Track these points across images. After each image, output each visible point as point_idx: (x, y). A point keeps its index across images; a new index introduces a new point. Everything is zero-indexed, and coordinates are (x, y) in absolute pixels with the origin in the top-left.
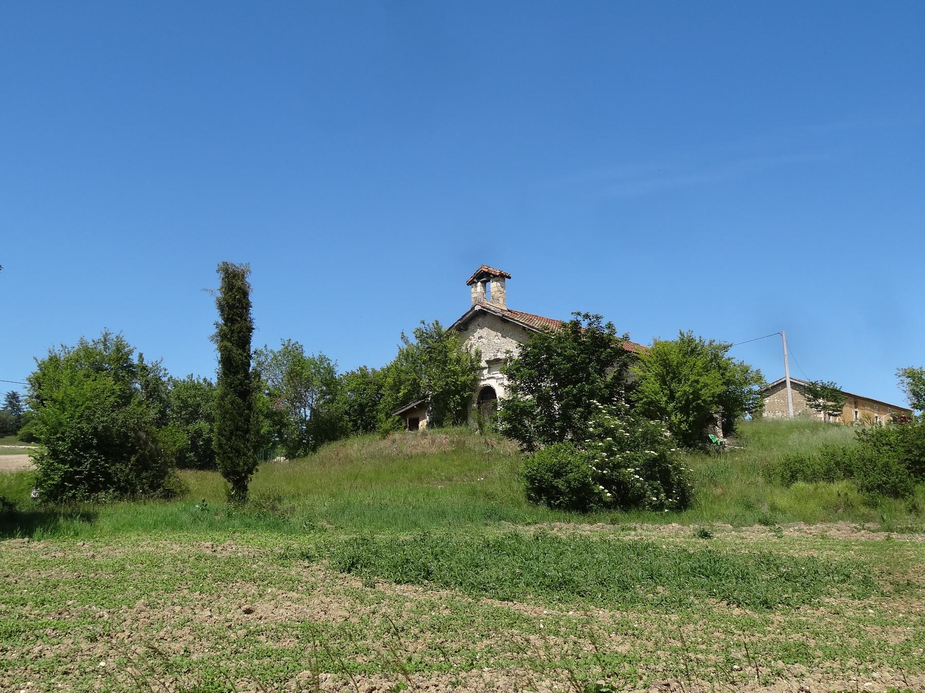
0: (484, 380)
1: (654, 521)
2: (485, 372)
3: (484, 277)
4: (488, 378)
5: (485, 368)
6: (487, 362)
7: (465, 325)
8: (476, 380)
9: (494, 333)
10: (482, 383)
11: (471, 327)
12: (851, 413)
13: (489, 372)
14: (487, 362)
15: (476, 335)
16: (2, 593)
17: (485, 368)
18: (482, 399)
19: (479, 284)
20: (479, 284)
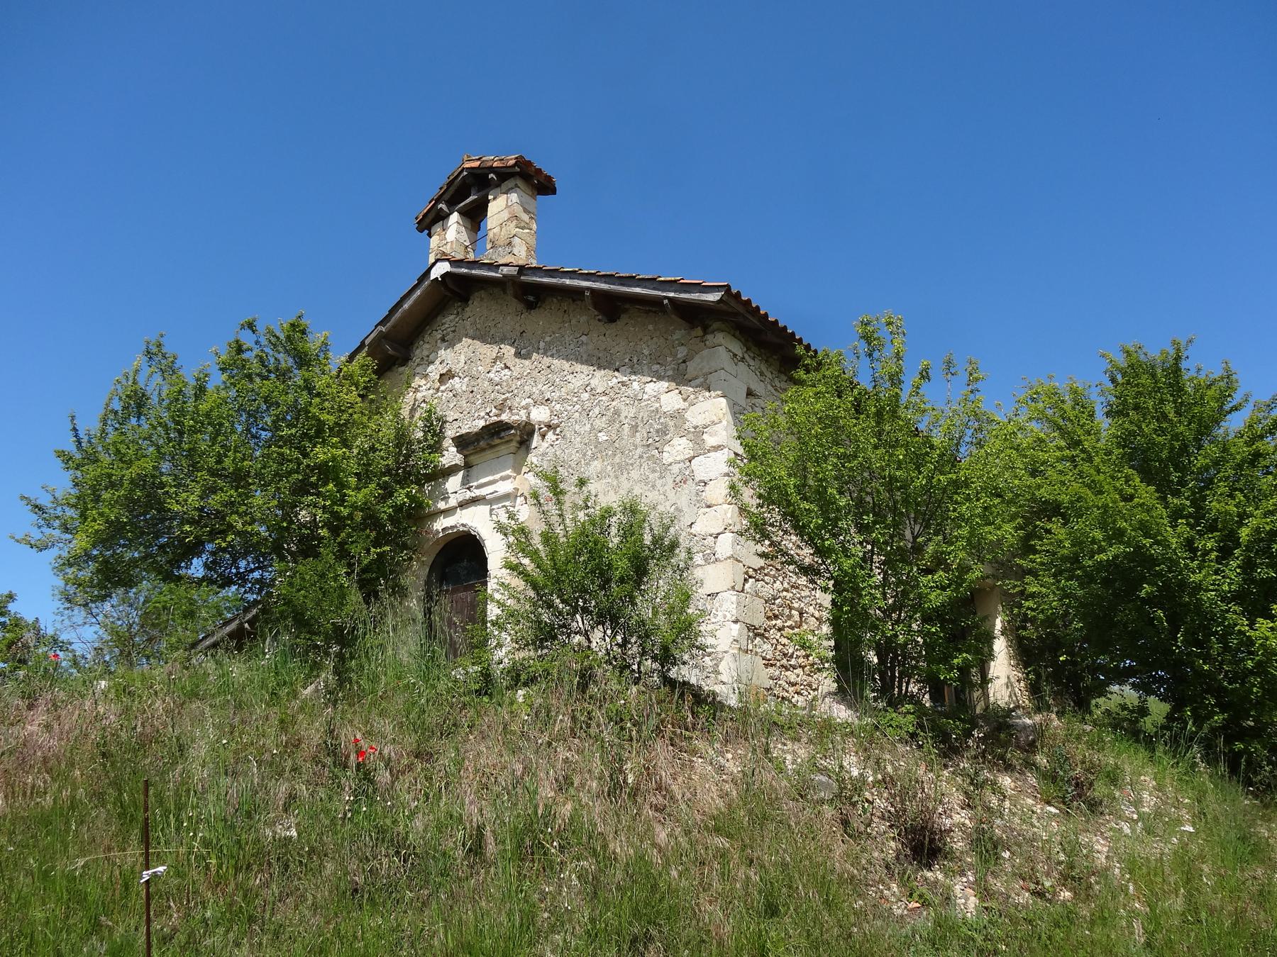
0: (448, 512)
1: (600, 361)
2: (453, 483)
3: (468, 193)
4: (463, 505)
5: (452, 470)
6: (463, 442)
7: (397, 347)
8: (418, 514)
9: (489, 351)
10: (440, 524)
11: (420, 351)
12: (142, 797)
13: (465, 483)
14: (463, 442)
15: (434, 370)
16: (1032, 950)
17: (452, 470)
18: (443, 579)
19: (455, 217)
20: (455, 217)
